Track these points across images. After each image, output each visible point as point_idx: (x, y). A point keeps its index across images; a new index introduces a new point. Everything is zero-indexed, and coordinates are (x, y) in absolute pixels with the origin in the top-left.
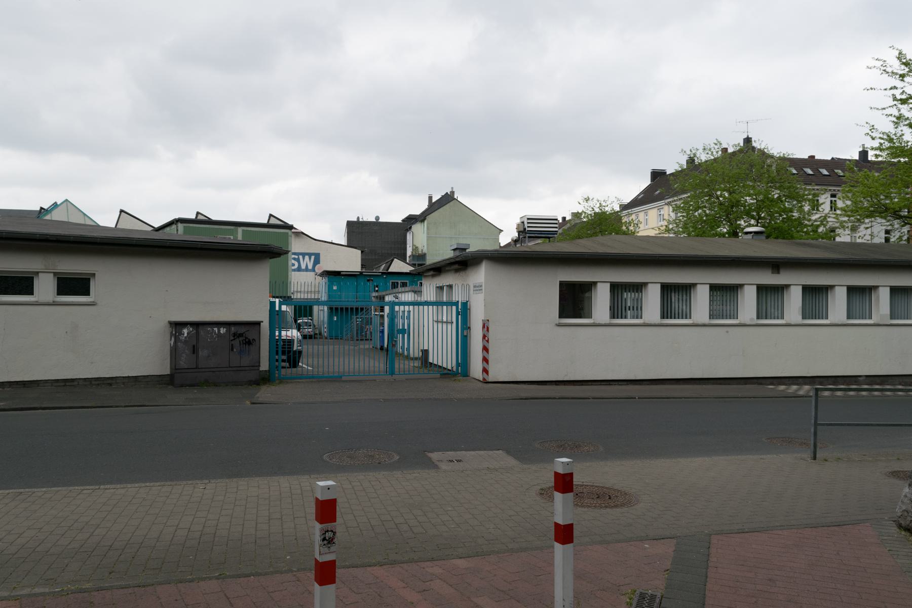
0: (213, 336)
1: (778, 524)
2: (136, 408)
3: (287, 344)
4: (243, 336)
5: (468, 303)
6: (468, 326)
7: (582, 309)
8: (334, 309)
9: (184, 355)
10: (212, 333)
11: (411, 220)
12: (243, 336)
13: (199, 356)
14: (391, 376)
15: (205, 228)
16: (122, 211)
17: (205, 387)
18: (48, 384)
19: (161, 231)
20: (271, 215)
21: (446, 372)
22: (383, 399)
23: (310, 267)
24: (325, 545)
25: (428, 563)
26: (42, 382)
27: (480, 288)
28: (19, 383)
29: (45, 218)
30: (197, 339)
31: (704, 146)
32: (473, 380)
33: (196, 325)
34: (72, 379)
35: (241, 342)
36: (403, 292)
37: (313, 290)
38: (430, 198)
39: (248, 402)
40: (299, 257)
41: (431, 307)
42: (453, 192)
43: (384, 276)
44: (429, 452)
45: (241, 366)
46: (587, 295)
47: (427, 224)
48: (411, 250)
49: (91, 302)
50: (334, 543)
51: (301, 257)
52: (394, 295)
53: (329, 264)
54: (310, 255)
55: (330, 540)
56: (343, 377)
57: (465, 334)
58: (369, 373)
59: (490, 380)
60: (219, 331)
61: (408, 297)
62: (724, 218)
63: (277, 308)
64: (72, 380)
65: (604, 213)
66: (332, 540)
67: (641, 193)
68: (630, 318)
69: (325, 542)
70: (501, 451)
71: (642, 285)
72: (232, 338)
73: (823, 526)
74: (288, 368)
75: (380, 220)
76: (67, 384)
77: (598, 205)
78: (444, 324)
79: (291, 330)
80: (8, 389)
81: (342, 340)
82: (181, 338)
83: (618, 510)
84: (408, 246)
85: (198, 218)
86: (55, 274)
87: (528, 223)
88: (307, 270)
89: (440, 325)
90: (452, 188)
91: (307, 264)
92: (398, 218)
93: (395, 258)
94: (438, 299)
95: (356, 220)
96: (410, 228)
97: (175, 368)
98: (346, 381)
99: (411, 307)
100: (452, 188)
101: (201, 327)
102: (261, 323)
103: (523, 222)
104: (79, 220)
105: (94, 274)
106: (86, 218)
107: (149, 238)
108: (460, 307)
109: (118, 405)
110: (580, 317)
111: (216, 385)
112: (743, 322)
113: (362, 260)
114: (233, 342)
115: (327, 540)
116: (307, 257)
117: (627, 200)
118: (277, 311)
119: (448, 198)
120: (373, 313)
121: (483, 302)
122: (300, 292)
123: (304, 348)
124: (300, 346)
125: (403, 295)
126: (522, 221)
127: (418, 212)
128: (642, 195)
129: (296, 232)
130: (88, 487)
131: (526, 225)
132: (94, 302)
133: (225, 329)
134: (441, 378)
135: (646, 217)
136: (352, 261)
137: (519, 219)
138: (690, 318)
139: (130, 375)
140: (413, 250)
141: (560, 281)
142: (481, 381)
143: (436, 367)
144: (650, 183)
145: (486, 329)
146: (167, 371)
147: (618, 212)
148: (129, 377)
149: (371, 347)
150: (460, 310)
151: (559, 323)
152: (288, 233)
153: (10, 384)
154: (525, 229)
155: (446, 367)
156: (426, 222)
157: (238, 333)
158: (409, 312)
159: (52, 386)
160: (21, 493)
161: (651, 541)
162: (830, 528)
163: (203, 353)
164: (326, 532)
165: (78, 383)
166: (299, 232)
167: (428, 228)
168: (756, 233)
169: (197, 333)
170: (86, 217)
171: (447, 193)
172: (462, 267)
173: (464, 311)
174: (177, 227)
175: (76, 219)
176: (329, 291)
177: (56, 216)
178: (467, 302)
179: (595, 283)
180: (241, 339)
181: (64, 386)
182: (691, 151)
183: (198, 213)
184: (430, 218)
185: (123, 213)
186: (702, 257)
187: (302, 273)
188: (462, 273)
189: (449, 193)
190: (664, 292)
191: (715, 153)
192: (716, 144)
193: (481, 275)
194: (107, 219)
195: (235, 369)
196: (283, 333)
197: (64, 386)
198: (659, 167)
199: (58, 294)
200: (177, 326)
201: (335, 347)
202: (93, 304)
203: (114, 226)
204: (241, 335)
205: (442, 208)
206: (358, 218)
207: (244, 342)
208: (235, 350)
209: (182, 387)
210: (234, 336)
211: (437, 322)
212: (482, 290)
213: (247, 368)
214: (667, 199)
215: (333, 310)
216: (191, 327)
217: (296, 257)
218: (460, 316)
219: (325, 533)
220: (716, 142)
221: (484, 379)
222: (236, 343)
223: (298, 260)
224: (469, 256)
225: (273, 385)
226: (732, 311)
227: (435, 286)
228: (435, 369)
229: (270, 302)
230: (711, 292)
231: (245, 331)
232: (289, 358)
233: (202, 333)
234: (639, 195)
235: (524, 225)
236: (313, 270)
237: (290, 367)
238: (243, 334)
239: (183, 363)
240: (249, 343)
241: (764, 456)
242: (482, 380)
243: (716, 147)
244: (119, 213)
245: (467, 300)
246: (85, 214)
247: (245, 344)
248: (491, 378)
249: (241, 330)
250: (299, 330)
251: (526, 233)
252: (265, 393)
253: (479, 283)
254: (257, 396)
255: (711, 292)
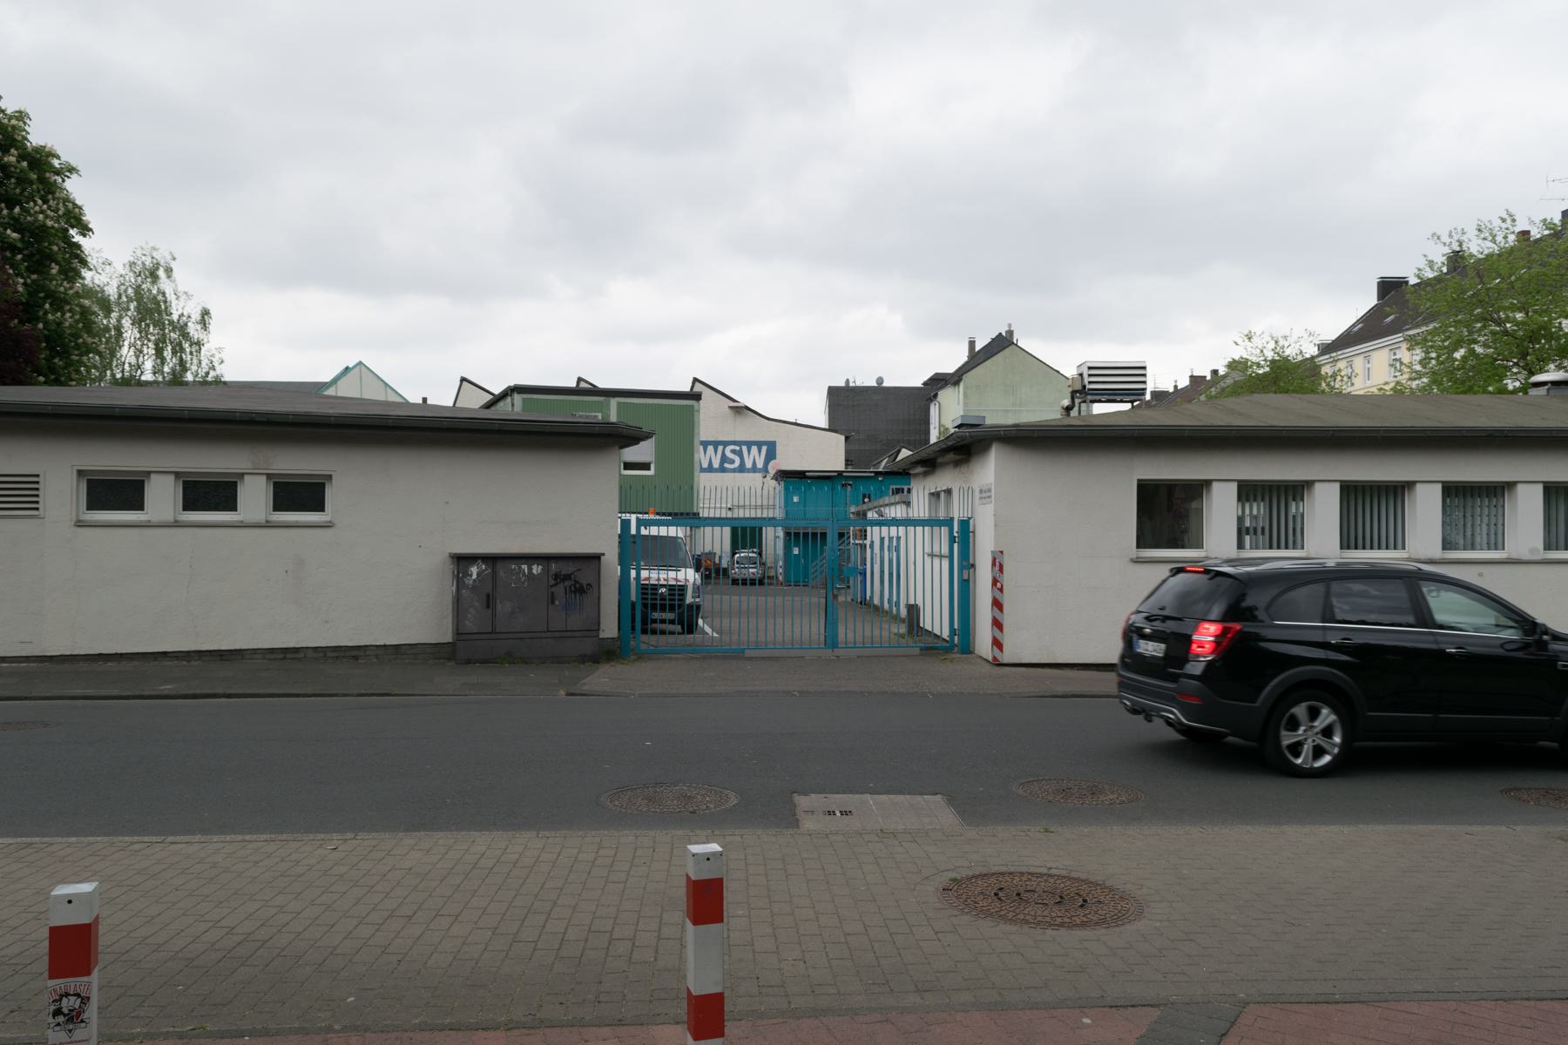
0: (520, 579)
1: (1419, 988)
2: (375, 698)
3: (649, 591)
4: (570, 579)
5: (971, 521)
6: (971, 562)
7: (1185, 531)
8: (801, 535)
9: (471, 610)
10: (518, 573)
11: (939, 382)
12: (570, 579)
13: (497, 612)
14: (831, 650)
15: (563, 400)
16: (463, 380)
17: (507, 665)
18: (257, 656)
19: (493, 408)
20: (696, 380)
21: (930, 641)
22: (799, 692)
23: (760, 465)
24: (58, 1024)
25: (607, 1029)
26: (249, 652)
27: (988, 494)
28: (213, 654)
29: (326, 393)
30: (494, 587)
31: (1478, 225)
32: (979, 660)
33: (492, 560)
34: (294, 648)
35: (568, 589)
36: (892, 504)
37: (765, 503)
38: (972, 344)
39: (562, 693)
40: (741, 449)
41: (919, 529)
42: (1010, 333)
43: (880, 479)
44: (800, 793)
45: (568, 629)
46: (1194, 505)
47: (964, 389)
48: (938, 435)
49: (326, 522)
50: (82, 1021)
51: (744, 448)
52: (877, 509)
53: (789, 460)
54: (759, 444)
55: (74, 1013)
56: (746, 651)
57: (966, 577)
58: (846, 644)
59: (1006, 661)
60: (530, 569)
61: (897, 512)
62: (1515, 360)
63: (633, 531)
64: (296, 650)
65: (1286, 359)
66: (79, 1014)
67: (1358, 322)
68: (1251, 548)
69: (61, 1019)
70: (939, 796)
71: (1303, 486)
72: (552, 582)
73: (1528, 999)
74: (679, 633)
75: (885, 384)
76: (288, 656)
77: (1272, 345)
78: (938, 554)
79: (683, 570)
80: (196, 663)
81: (806, 588)
82: (467, 581)
83: (1080, 933)
84: (932, 427)
85: (581, 386)
86: (269, 476)
87: (1090, 375)
88: (754, 469)
89: (936, 561)
90: (1010, 325)
91: (754, 459)
92: (917, 381)
93: (903, 447)
94: (933, 515)
95: (843, 384)
96: (936, 396)
97: (458, 633)
98: (751, 659)
99: (902, 529)
100: (1010, 325)
101: (499, 565)
102: (602, 557)
103: (1081, 375)
104: (378, 395)
105: (331, 476)
106: (389, 391)
107: (431, 415)
108: (956, 529)
109: (347, 692)
110: (1183, 547)
111: (525, 661)
112: (1514, 556)
113: (847, 452)
114: (553, 589)
115: (65, 1015)
116: (754, 449)
117: (1331, 334)
118: (634, 536)
119: (1003, 342)
120: (852, 541)
121: (992, 518)
122: (744, 507)
123: (706, 601)
124: (699, 597)
125: (893, 508)
126: (1080, 372)
127: (950, 368)
128: (1360, 326)
129: (737, 407)
130: (140, 839)
131: (1087, 380)
132: (330, 522)
133: (540, 567)
134: (921, 655)
135: (1368, 366)
136: (829, 455)
137: (1075, 369)
138: (1404, 548)
139: (387, 643)
140: (940, 433)
141: (1138, 480)
142: (988, 661)
143: (930, 636)
144: (1375, 302)
145: (997, 568)
146: (448, 637)
147: (1313, 358)
148: (385, 646)
149: (849, 599)
150: (956, 535)
151: (1137, 558)
152: (693, 406)
153: (200, 654)
154: (1084, 387)
155: (939, 634)
156: (962, 385)
157: (563, 573)
158: (899, 538)
159: (264, 658)
160: (31, 844)
161: (1106, 1009)
162: (1542, 1005)
163: (504, 607)
164: (62, 996)
165: (305, 654)
166: (741, 407)
167: (965, 396)
168: (1555, 384)
169: (494, 574)
170: (388, 389)
171: (1000, 334)
172: (963, 457)
173: (964, 535)
174: (512, 400)
175: (373, 393)
176: (786, 506)
177: (346, 390)
178: (970, 518)
179: (1207, 483)
180: (567, 583)
181: (282, 659)
182: (1450, 236)
183: (580, 380)
184: (969, 378)
185: (464, 383)
186: (1423, 430)
187: (746, 475)
188: (964, 469)
189: (1004, 334)
190: (1348, 496)
191: (1499, 239)
192: (1504, 220)
193: (990, 469)
194: (443, 397)
195: (557, 634)
196: (644, 574)
197: (282, 659)
198: (1393, 272)
199: (186, 508)
200: (462, 561)
201: (795, 599)
202: (328, 525)
203: (451, 405)
204: (567, 577)
205: (990, 360)
206: (848, 381)
207: (573, 588)
208: (557, 602)
209: (469, 663)
210: (555, 579)
211: (932, 555)
212: (990, 497)
213: (578, 634)
214: (1407, 330)
215: (792, 537)
216: (483, 562)
217: (738, 448)
218: (956, 545)
219: (60, 1000)
220: (1505, 216)
221: (995, 659)
222: (560, 590)
223: (740, 453)
224: (966, 436)
225: (622, 664)
226: (1493, 536)
227: (927, 492)
228: (927, 638)
229: (622, 520)
230: (1448, 500)
231: (575, 569)
232: (681, 616)
233: (501, 573)
234: (1354, 325)
235: (1082, 379)
236: (765, 470)
237: (683, 633)
238: (570, 575)
239: (471, 625)
240: (580, 590)
241: (1475, 829)
242: (990, 659)
243: (1504, 225)
244: (459, 383)
245: (970, 516)
246: (386, 384)
247: (575, 592)
248: (1007, 657)
249: (568, 568)
250: (697, 570)
251: (1087, 394)
252: (602, 678)
253: (987, 485)
254: (584, 681)
255: (1448, 500)
